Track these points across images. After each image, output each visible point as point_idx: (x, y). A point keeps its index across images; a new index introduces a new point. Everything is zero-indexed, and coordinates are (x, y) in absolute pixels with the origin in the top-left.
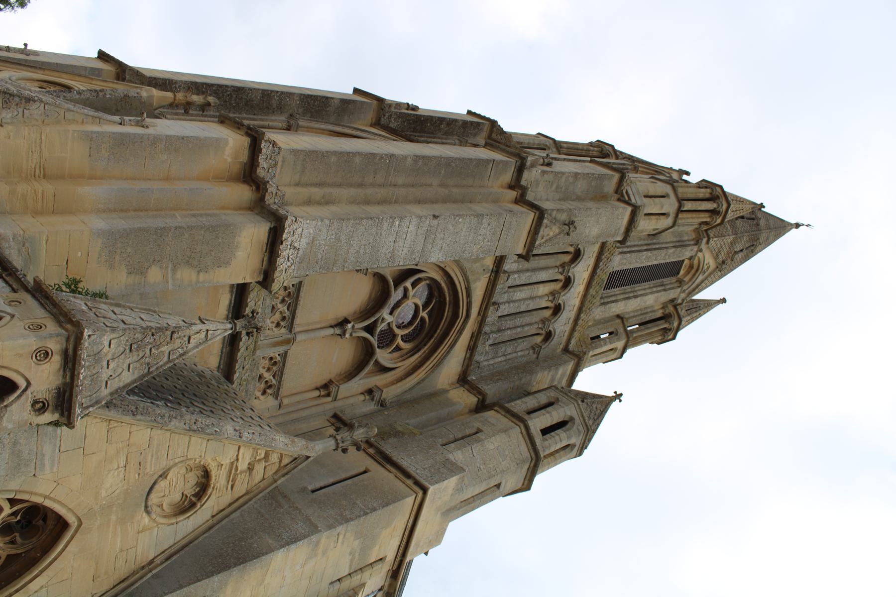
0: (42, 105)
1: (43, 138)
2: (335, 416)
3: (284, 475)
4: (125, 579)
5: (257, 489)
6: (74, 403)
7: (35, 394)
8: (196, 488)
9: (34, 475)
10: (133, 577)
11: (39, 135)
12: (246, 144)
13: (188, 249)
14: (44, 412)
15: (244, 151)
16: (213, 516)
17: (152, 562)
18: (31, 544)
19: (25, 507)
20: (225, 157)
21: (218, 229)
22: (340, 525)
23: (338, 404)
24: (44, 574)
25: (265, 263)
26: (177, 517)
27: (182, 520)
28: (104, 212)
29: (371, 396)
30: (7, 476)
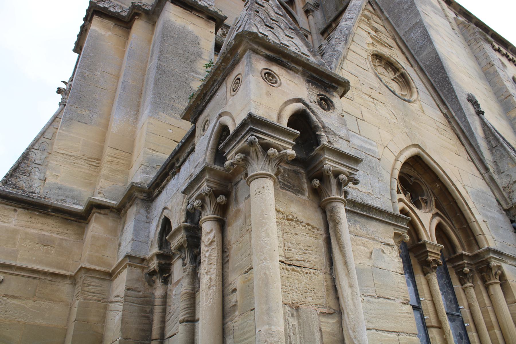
0: (33, 150)
1: (62, 152)
2: (323, 33)
3: (382, 12)
4: (457, 136)
5: (392, 33)
6: (325, 70)
7: (312, 100)
8: (389, 70)
9: (379, 159)
10: (456, 130)
11: (60, 155)
12: (98, 19)
13: (180, 58)
14: (332, 102)
15: (104, 22)
16: (412, 66)
17: (445, 115)
18: (428, 190)
19: (400, 185)
20: (107, 35)
21: (166, 34)
22: (417, 8)
23: (313, 31)
24: (455, 184)
25: (201, 16)
26: (411, 87)
27: (415, 84)
28: (137, 118)
29: (310, 11)
30: (379, 178)
